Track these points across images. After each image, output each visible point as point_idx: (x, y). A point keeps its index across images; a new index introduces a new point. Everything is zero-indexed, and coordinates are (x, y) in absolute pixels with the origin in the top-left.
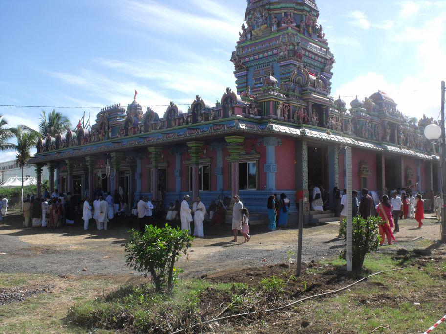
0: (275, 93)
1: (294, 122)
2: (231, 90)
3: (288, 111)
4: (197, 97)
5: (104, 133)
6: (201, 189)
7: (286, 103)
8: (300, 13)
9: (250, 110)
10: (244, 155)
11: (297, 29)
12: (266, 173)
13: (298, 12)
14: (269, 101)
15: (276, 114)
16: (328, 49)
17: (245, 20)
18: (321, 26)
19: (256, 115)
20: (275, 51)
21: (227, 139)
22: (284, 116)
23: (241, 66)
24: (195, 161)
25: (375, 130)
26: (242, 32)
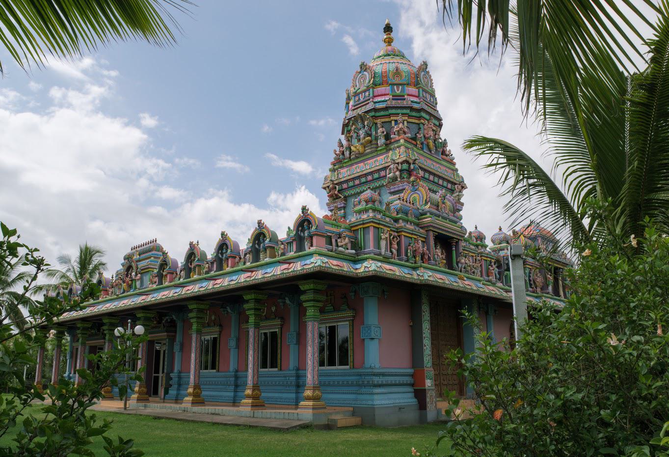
0: (379, 216)
1: (407, 261)
2: (308, 210)
3: (399, 244)
5: (130, 282)
7: (394, 231)
8: (417, 121)
9: (339, 240)
11: (413, 142)
12: (364, 340)
13: (413, 121)
14: (369, 227)
15: (379, 247)
16: (457, 170)
17: (343, 133)
18: (445, 140)
19: (347, 249)
20: (383, 173)
22: (391, 252)
23: (336, 195)
24: (253, 321)
25: (530, 276)
26: (338, 149)
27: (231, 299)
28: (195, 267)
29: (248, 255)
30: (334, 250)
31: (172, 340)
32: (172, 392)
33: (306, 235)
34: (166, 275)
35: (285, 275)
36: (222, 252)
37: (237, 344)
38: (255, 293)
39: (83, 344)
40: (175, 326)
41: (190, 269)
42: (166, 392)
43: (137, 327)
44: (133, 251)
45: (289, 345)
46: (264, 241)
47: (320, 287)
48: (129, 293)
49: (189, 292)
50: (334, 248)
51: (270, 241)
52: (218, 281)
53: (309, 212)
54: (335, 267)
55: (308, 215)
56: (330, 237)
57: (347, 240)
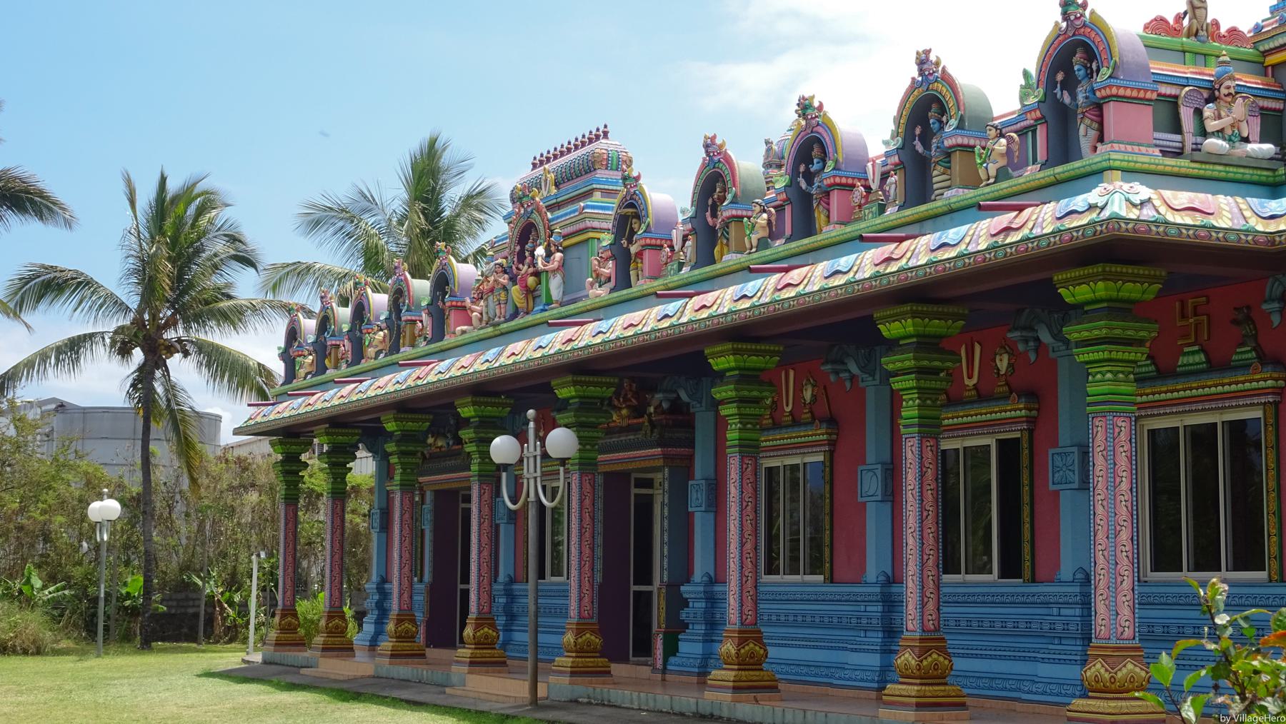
4: (923, 61)
5: (531, 281)
6: (986, 569)
10: (1150, 379)
19: (1247, 140)
21: (1066, 283)
27: (835, 333)
28: (726, 225)
29: (892, 180)
30: (1188, 147)
31: (682, 470)
32: (690, 647)
33: (1081, 98)
34: (639, 254)
35: (1000, 254)
36: (807, 169)
37: (885, 486)
38: (914, 315)
39: (407, 487)
40: (689, 425)
41: (712, 231)
42: (671, 649)
43: (497, 440)
44: (540, 170)
45: (1057, 493)
46: (942, 125)
47: (1131, 290)
48: (529, 319)
49: (791, 293)
50: (1190, 139)
51: (960, 126)
52: (795, 276)
53: (1087, 13)
54: (1188, 220)
55: (1085, 25)
56: (1173, 102)
57: (1239, 108)
